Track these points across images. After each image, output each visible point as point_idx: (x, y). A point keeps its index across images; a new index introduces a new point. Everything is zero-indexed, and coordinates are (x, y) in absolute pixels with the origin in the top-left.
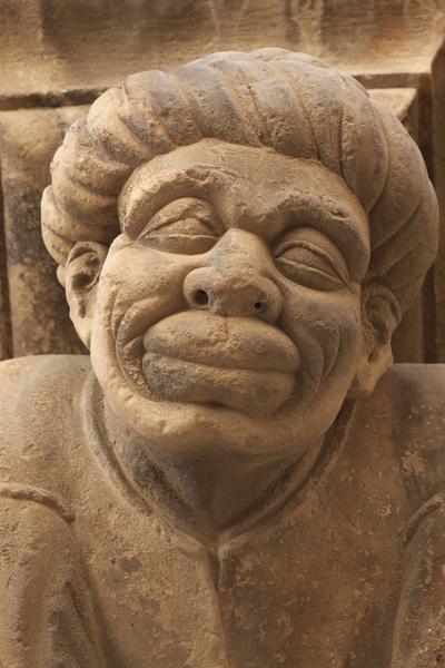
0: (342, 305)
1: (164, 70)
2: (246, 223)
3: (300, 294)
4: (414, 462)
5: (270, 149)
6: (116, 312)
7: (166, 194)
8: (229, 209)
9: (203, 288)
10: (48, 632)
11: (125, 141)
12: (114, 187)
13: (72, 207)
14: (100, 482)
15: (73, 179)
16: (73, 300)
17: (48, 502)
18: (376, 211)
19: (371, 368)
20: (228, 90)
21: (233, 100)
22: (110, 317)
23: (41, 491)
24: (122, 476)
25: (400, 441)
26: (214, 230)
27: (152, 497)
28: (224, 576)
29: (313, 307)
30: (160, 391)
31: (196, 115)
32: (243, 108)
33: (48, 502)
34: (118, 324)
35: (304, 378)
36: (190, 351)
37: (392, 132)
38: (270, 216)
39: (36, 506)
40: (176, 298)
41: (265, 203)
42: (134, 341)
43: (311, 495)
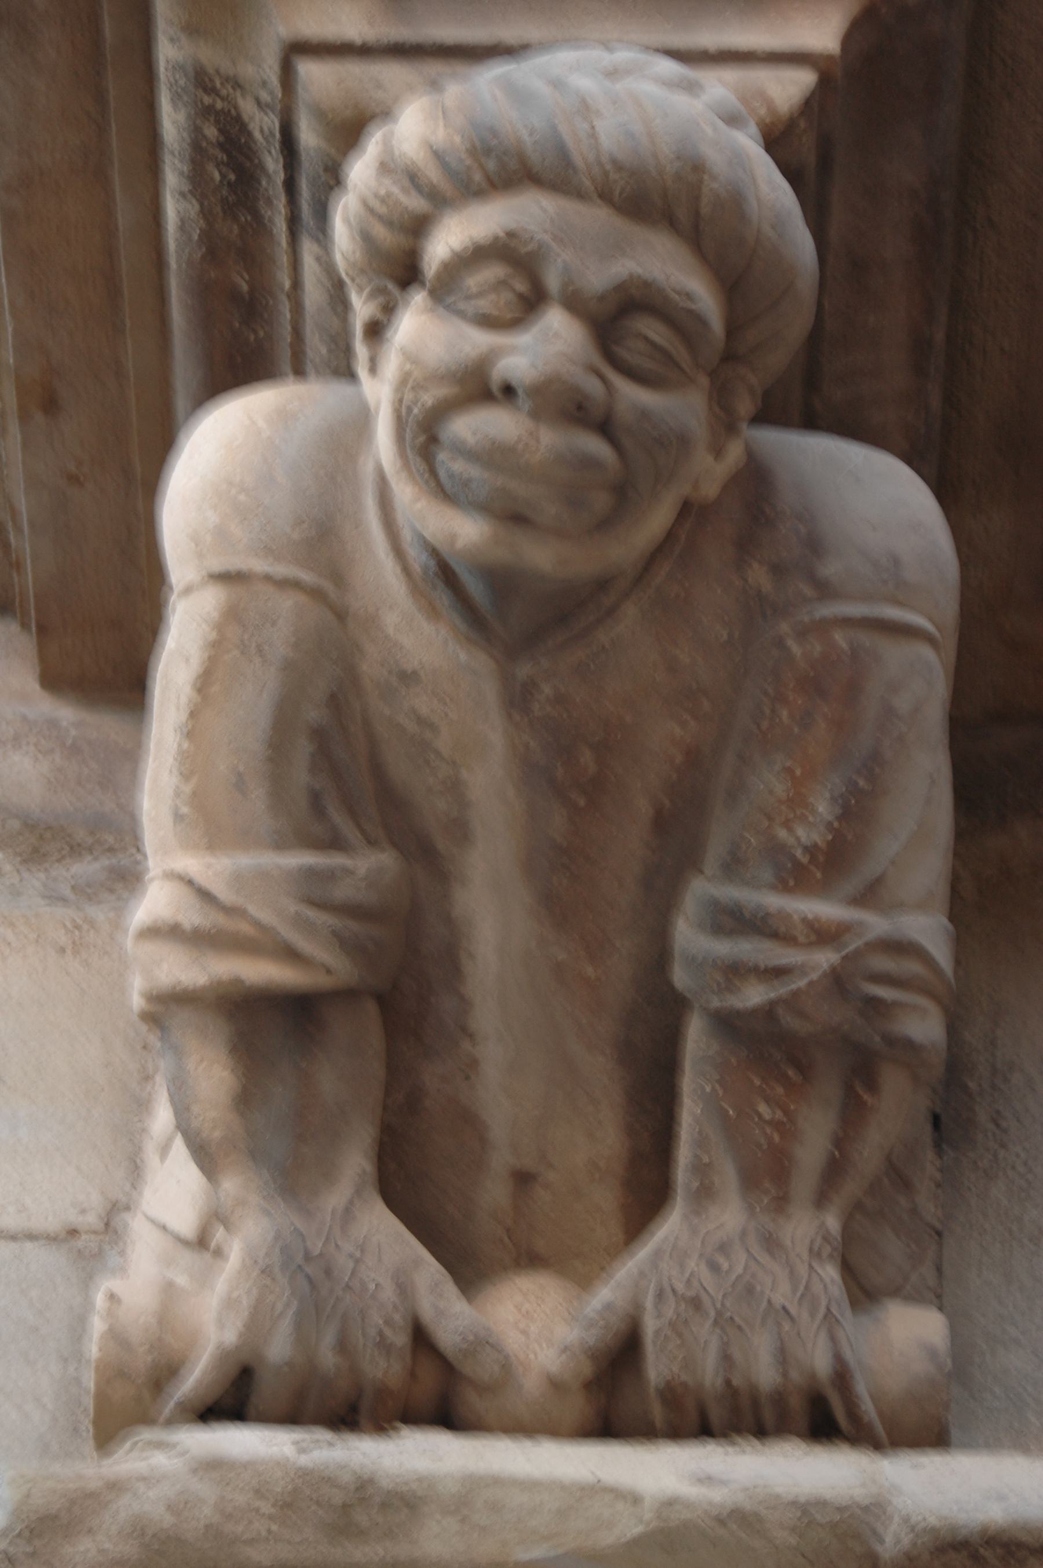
0: (683, 408)
1: (455, 788)
2: (574, 303)
3: (632, 395)
4: (759, 576)
5: (244, 1537)
6: (408, 396)
7: (477, 255)
8: (553, 282)
9: (514, 383)
10: (303, 749)
11: (435, 181)
12: (418, 227)
13: (366, 238)
14: (383, 581)
15: (371, 211)
16: (361, 350)
17: (316, 594)
18: (733, 285)
19: (710, 473)
20: (564, 130)
21: (570, 143)
22: (401, 401)
23: (306, 577)
24: (406, 570)
25: (745, 546)
26: (532, 302)
27: (443, 598)
28: (517, 699)
29: (644, 414)
30: (444, 491)
31: (522, 158)
32: (580, 154)
33: (316, 594)
34: (409, 409)
35: (624, 496)
36: (494, 456)
37: (764, 188)
38: (602, 298)
39: (302, 598)
40: (478, 387)
41: (599, 276)
42: (423, 437)
43: (630, 611)
